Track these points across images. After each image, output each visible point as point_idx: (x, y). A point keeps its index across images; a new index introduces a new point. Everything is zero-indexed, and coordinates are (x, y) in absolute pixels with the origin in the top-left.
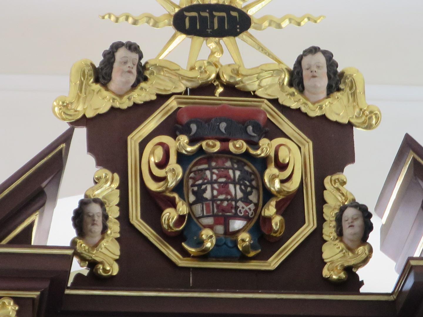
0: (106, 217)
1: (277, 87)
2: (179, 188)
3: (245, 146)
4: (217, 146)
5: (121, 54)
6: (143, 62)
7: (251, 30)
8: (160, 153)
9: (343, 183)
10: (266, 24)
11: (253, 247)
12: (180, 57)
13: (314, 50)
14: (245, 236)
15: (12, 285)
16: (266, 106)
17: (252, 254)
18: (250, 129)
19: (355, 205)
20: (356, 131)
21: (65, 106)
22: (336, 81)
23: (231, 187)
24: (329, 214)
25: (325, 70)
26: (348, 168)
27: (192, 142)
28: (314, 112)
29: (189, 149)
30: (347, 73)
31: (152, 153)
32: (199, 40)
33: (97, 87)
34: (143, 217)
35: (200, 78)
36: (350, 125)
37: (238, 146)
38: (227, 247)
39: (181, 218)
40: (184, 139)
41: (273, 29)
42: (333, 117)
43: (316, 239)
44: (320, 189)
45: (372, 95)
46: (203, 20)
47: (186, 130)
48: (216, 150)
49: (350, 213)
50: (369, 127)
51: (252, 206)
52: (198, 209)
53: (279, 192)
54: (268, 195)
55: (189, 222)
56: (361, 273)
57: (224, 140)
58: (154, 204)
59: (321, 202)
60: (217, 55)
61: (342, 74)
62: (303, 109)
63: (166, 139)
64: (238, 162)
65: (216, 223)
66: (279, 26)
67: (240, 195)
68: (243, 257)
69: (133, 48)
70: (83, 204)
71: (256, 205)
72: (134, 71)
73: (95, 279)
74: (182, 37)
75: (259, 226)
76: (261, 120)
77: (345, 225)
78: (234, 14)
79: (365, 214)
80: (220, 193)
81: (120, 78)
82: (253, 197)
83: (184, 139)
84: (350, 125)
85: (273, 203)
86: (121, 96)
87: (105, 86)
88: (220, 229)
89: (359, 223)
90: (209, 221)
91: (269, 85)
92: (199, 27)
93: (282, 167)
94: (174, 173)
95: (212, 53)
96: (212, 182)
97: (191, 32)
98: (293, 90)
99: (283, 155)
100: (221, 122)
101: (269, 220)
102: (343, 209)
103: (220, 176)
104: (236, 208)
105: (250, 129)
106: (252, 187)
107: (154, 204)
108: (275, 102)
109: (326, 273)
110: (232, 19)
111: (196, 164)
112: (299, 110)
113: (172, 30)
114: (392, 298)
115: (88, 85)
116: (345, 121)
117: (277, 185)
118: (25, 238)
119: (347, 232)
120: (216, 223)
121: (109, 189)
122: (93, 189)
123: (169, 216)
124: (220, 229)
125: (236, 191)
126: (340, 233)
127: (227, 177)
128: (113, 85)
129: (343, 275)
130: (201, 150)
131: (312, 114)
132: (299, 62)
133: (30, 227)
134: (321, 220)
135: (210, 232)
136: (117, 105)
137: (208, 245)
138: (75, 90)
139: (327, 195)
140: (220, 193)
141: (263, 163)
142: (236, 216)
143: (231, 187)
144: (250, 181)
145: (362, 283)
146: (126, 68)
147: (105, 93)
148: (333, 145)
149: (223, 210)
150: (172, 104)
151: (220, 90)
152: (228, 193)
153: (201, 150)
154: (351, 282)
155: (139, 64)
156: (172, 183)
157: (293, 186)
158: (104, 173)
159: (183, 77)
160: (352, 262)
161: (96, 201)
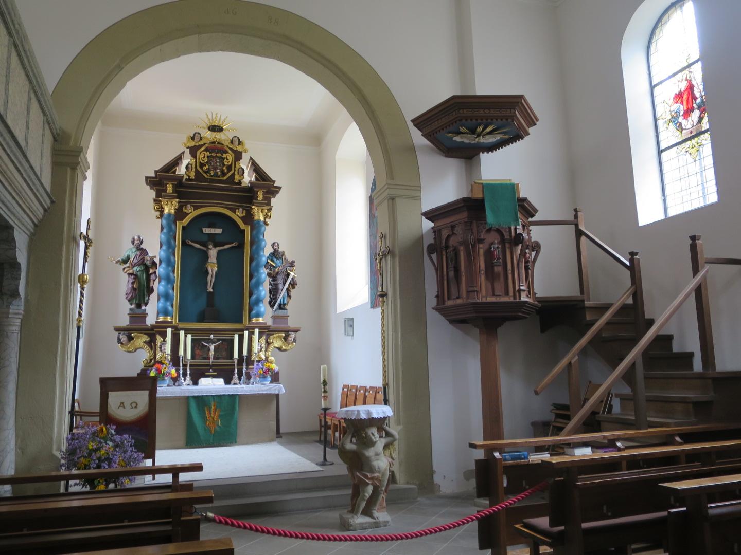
0: (192, 167)
2: (207, 163)
4: (215, 155)
5: (196, 135)
12: (208, 135)
13: (235, 137)
20: (243, 153)
21: (185, 144)
22: (240, 143)
24: (237, 169)
26: (241, 160)
32: (213, 133)
33: (192, 141)
35: (212, 141)
37: (219, 155)
38: (216, 174)
39: (207, 169)
40: (208, 153)
43: (233, 174)
44: (235, 164)
47: (209, 151)
49: (240, 170)
52: (210, 167)
54: (224, 165)
56: (242, 181)
59: (235, 167)
63: (205, 152)
68: (219, 177)
69: (199, 133)
73: (189, 179)
74: (209, 132)
75: (222, 171)
81: (196, 139)
83: (208, 153)
89: (242, 172)
91: (227, 143)
92: (562, 525)
93: (227, 160)
94: (206, 160)
100: (216, 149)
107: (202, 165)
108: (227, 146)
117: (226, 163)
118: (175, 172)
119: (240, 173)
123: (205, 168)
125: (218, 164)
128: (195, 141)
132: (232, 139)
134: (235, 170)
141: (224, 159)
142: (218, 169)
148: (238, 156)
150: (207, 145)
154: (240, 183)
156: (205, 161)
157: (230, 163)
158: (193, 158)
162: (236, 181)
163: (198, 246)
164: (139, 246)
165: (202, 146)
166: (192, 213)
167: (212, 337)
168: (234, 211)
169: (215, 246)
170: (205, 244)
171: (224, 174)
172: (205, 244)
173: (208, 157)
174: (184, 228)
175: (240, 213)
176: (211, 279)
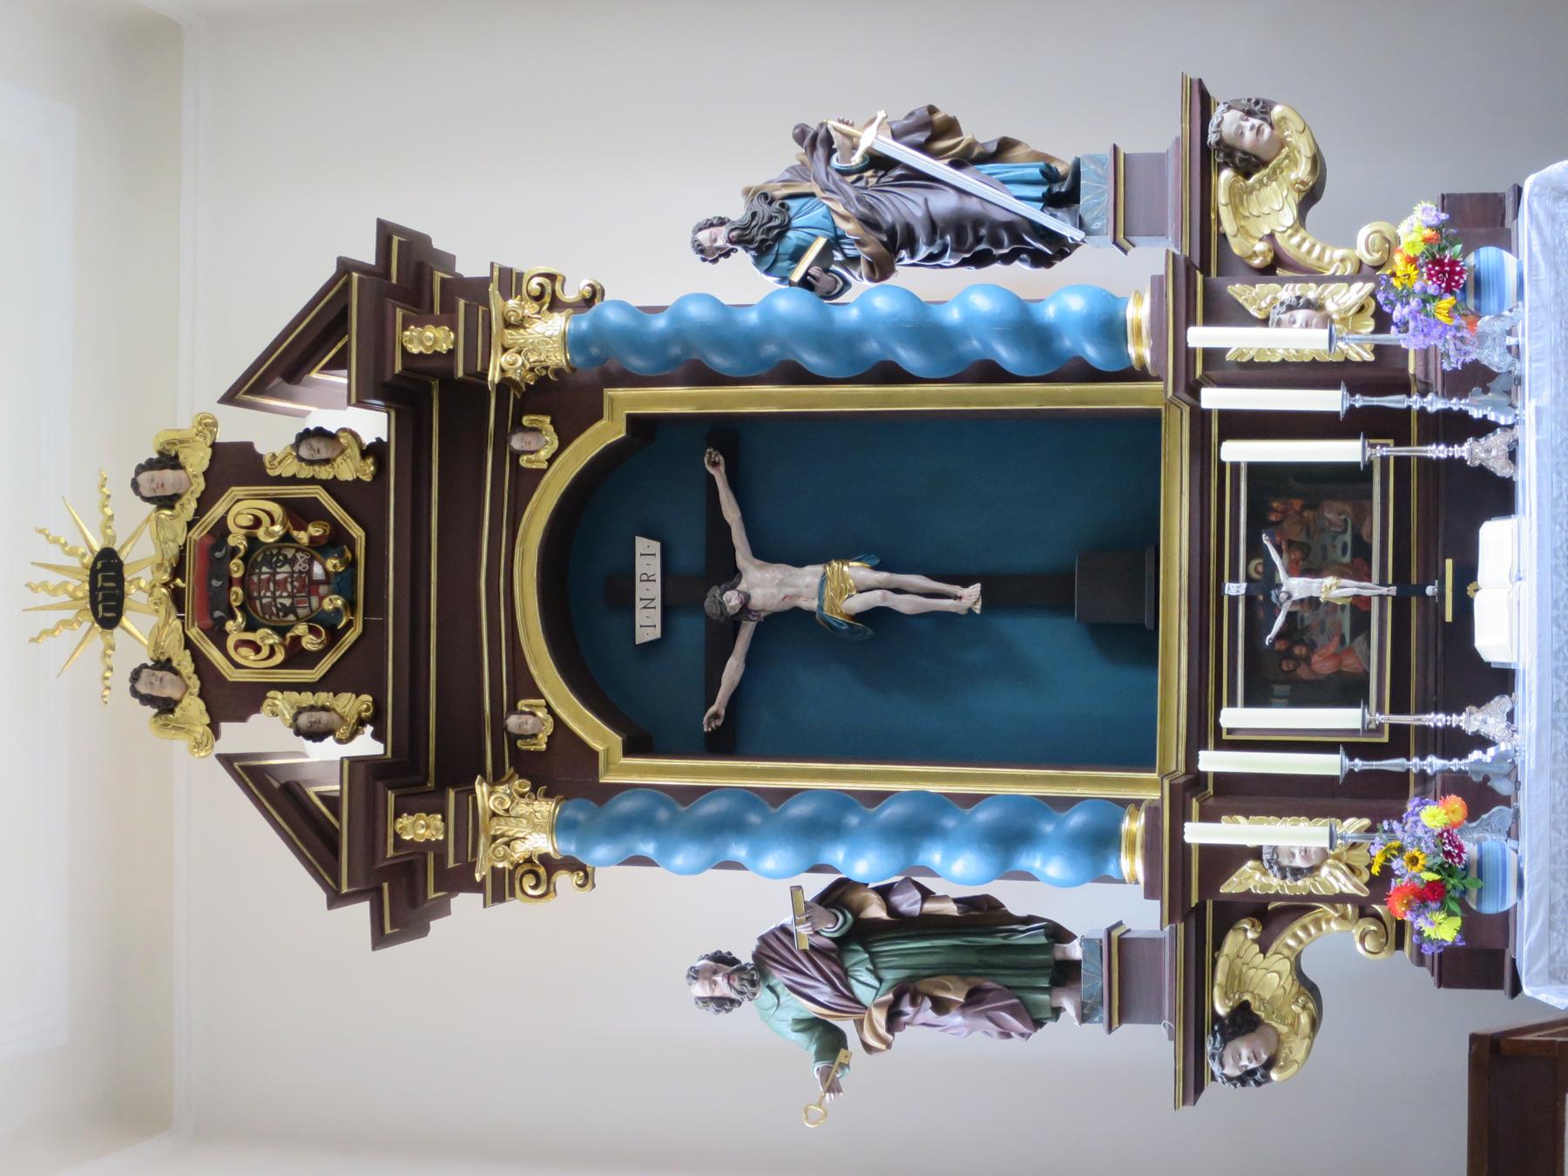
0: (312, 708)
1: (175, 522)
2: (281, 631)
3: (236, 560)
4: (237, 589)
5: (143, 688)
6: (150, 663)
7: (116, 547)
8: (244, 651)
9: (274, 456)
10: (109, 532)
11: (341, 556)
12: (146, 625)
13: (135, 485)
14: (331, 563)
15: (381, 812)
16: (196, 534)
17: (349, 555)
18: (218, 555)
19: (296, 446)
22: (168, 460)
23: (279, 577)
24: (306, 472)
25: (155, 473)
26: (259, 449)
27: (234, 617)
28: (200, 484)
29: (240, 619)
30: (159, 447)
31: (246, 658)
34: (312, 668)
36: (214, 446)
37: (236, 568)
38: (342, 583)
39: (312, 630)
40: (230, 625)
41: (114, 524)
42: (206, 464)
43: (332, 486)
44: (279, 481)
45: (184, 423)
46: (105, 598)
47: (221, 623)
48: (240, 591)
49: (304, 452)
50: (215, 425)
51: (299, 555)
52: (302, 612)
53: (284, 525)
54: (287, 538)
55: (319, 621)
56: (368, 439)
57: (231, 582)
58: (297, 657)
59: (294, 480)
60: (143, 584)
61: (160, 453)
62: (198, 495)
63: (230, 643)
64: (253, 567)
65: (317, 593)
66: (111, 518)
67: (287, 568)
68: (352, 564)
69: (136, 676)
70: (298, 732)
71: (298, 550)
72: (159, 674)
74: (125, 621)
75: (319, 548)
76: (210, 542)
77: (317, 457)
78: (99, 565)
79: (305, 436)
80: (285, 589)
81: (169, 690)
82: (290, 553)
83: (230, 625)
84: (214, 446)
85: (295, 533)
86: (187, 687)
87: (176, 703)
88: (323, 589)
89: (315, 443)
90: (314, 601)
91: (176, 527)
93: (257, 522)
95: (140, 588)
96: (274, 598)
97: (119, 614)
98: (177, 506)
99: (246, 520)
100: (212, 582)
101: (312, 539)
102: (301, 459)
103: (268, 589)
104: (300, 572)
105: (218, 555)
106: (279, 554)
107: (297, 657)
108: (190, 525)
109: (367, 478)
110: (103, 569)
111: (255, 611)
112: (198, 500)
113: (117, 631)
114: (393, 414)
115: (176, 721)
116: (209, 451)
117: (277, 528)
118: (332, 802)
119: (324, 455)
120: (317, 593)
121: (282, 702)
122: (284, 719)
123: (310, 643)
124: (323, 589)
125: (283, 572)
126: (327, 461)
127: (268, 581)
128: (176, 695)
129: (370, 461)
130: (241, 608)
131: (202, 486)
133: (322, 797)
134: (312, 481)
135: (326, 601)
136: (196, 691)
137: (339, 603)
138: (181, 735)
139: (287, 473)
140: (285, 589)
141: (252, 541)
142: (310, 572)
143: (279, 577)
144: (272, 556)
145: (379, 440)
146: (157, 683)
147: (184, 703)
148: (235, 465)
149: (303, 586)
150: (194, 633)
151: (178, 581)
152: (285, 580)
153: (241, 608)
154: (375, 451)
155: (152, 668)
156: (274, 639)
158: (266, 707)
159: (166, 623)
160: (357, 452)
161: (295, 718)
162: (367, 470)
163: (733, 670)
164: (741, 973)
165: (198, 657)
166: (555, 704)
167: (1235, 589)
168: (527, 481)
169: (731, 575)
170: (724, 631)
171: (336, 540)
172: (724, 631)
173: (251, 626)
174: (630, 749)
175: (536, 443)
176: (911, 596)
